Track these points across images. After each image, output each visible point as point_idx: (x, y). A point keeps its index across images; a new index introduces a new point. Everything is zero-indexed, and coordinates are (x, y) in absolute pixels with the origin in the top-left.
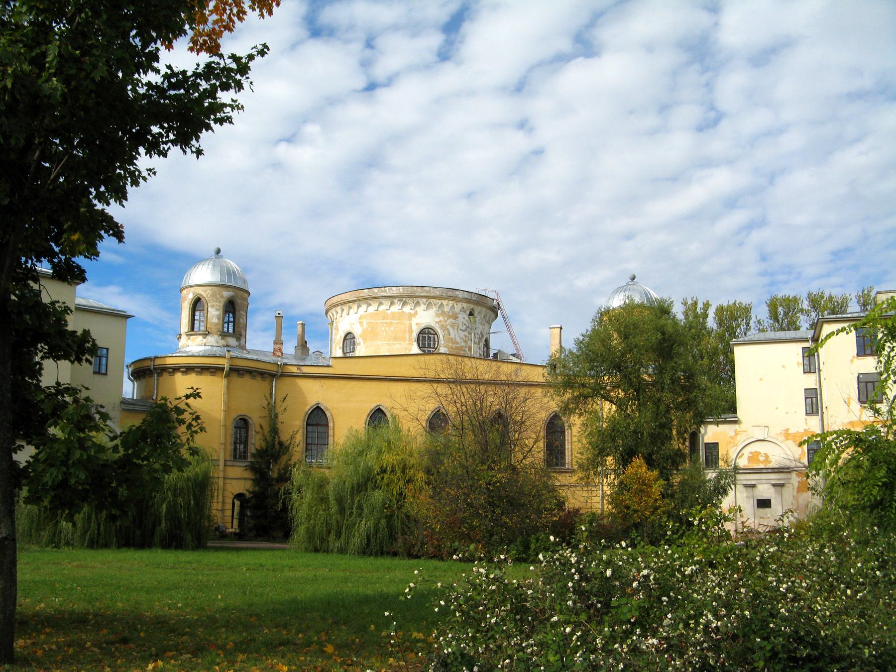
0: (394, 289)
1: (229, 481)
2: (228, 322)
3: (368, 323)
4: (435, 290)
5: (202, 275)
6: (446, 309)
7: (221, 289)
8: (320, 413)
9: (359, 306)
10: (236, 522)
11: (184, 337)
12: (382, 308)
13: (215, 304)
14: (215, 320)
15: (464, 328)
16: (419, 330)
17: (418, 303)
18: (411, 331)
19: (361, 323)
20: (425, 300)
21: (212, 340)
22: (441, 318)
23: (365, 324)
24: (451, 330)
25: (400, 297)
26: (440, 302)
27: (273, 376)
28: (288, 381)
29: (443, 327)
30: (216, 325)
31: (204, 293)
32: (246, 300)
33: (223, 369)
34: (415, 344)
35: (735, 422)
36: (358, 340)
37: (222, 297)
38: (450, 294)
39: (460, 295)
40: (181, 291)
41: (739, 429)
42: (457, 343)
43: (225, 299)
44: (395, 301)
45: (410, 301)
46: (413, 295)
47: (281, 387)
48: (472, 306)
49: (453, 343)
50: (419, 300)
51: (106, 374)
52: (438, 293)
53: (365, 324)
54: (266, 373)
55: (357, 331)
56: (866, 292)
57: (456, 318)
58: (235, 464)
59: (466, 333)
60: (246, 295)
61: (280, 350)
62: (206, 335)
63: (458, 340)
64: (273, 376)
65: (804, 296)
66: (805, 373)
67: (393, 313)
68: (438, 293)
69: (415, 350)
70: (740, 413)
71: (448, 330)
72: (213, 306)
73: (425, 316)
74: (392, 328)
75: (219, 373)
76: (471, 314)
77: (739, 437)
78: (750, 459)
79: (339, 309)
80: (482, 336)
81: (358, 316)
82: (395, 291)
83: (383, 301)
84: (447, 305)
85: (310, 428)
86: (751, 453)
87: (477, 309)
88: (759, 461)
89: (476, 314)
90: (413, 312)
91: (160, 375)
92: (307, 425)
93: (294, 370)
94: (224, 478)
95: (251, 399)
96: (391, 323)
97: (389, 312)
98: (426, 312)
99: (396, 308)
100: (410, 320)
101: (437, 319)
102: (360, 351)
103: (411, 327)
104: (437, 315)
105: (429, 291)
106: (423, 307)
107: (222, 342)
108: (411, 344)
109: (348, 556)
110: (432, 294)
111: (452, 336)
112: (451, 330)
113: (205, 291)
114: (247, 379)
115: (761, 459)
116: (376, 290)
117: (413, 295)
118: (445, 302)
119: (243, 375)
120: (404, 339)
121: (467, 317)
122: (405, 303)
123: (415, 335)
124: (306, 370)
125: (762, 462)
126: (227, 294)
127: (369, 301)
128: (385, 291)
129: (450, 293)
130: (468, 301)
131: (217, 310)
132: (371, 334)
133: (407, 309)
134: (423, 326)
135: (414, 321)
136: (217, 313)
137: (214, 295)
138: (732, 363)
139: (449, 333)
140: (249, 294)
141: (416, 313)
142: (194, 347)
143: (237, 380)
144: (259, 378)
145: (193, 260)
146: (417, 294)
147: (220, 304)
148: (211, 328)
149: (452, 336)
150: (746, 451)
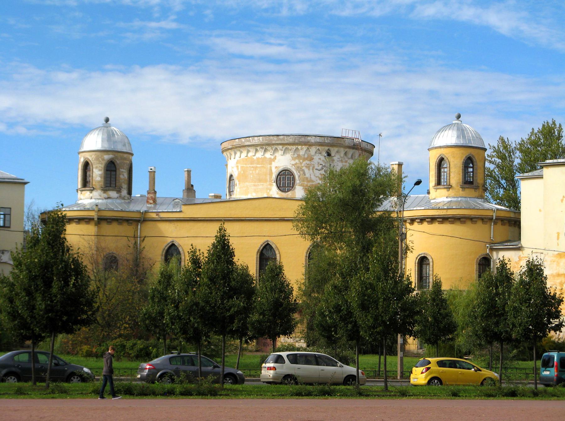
0: (256, 138)
3: (242, 167)
4: (289, 138)
5: (94, 142)
6: (302, 153)
7: (102, 153)
9: (235, 153)
12: (250, 154)
13: (98, 165)
14: (98, 179)
16: (278, 173)
17: (276, 150)
18: (271, 173)
19: (237, 167)
20: (281, 147)
21: (96, 194)
22: (297, 161)
23: (239, 167)
24: (306, 171)
25: (261, 145)
26: (294, 147)
27: (138, 221)
28: (150, 224)
29: (299, 169)
30: (99, 182)
31: (91, 157)
34: (275, 184)
35: (519, 249)
37: (103, 160)
38: (301, 141)
39: (313, 140)
40: (79, 153)
41: (522, 256)
42: (313, 181)
44: (258, 148)
45: (269, 148)
46: (271, 143)
47: (147, 229)
48: (327, 148)
49: (308, 182)
50: (276, 146)
51: (9, 227)
52: (291, 140)
53: (239, 167)
54: (475, 218)
57: (311, 159)
62: (449, 188)
63: (313, 178)
64: (138, 221)
66: (268, 244)
67: (258, 159)
68: (291, 140)
69: (275, 192)
70: (524, 242)
71: (303, 170)
72: (96, 168)
73: (283, 160)
74: (257, 172)
76: (329, 155)
81: (236, 160)
82: (256, 141)
83: (250, 149)
84: (303, 150)
90: (272, 157)
93: (154, 216)
95: (117, 241)
96: (256, 167)
97: (255, 158)
98: (283, 157)
99: (260, 154)
100: (271, 164)
101: (293, 162)
104: (294, 159)
105: (283, 139)
106: (280, 152)
107: (105, 195)
108: (271, 185)
110: (286, 142)
111: (307, 175)
112: (306, 171)
113: (91, 156)
116: (243, 140)
117: (271, 143)
118: (299, 147)
120: (266, 181)
122: (266, 151)
123: (274, 176)
124: (163, 215)
126: (107, 157)
128: (249, 141)
129: (303, 139)
130: (321, 144)
131: (100, 170)
132: (244, 176)
133: (268, 155)
134: (281, 169)
135: (274, 165)
136: (100, 173)
137: (97, 159)
139: (304, 174)
140: (132, 154)
141: (275, 158)
142: (88, 199)
143: (105, 226)
144: (125, 224)
145: (84, 130)
146: (274, 142)
147: (102, 166)
149: (307, 175)
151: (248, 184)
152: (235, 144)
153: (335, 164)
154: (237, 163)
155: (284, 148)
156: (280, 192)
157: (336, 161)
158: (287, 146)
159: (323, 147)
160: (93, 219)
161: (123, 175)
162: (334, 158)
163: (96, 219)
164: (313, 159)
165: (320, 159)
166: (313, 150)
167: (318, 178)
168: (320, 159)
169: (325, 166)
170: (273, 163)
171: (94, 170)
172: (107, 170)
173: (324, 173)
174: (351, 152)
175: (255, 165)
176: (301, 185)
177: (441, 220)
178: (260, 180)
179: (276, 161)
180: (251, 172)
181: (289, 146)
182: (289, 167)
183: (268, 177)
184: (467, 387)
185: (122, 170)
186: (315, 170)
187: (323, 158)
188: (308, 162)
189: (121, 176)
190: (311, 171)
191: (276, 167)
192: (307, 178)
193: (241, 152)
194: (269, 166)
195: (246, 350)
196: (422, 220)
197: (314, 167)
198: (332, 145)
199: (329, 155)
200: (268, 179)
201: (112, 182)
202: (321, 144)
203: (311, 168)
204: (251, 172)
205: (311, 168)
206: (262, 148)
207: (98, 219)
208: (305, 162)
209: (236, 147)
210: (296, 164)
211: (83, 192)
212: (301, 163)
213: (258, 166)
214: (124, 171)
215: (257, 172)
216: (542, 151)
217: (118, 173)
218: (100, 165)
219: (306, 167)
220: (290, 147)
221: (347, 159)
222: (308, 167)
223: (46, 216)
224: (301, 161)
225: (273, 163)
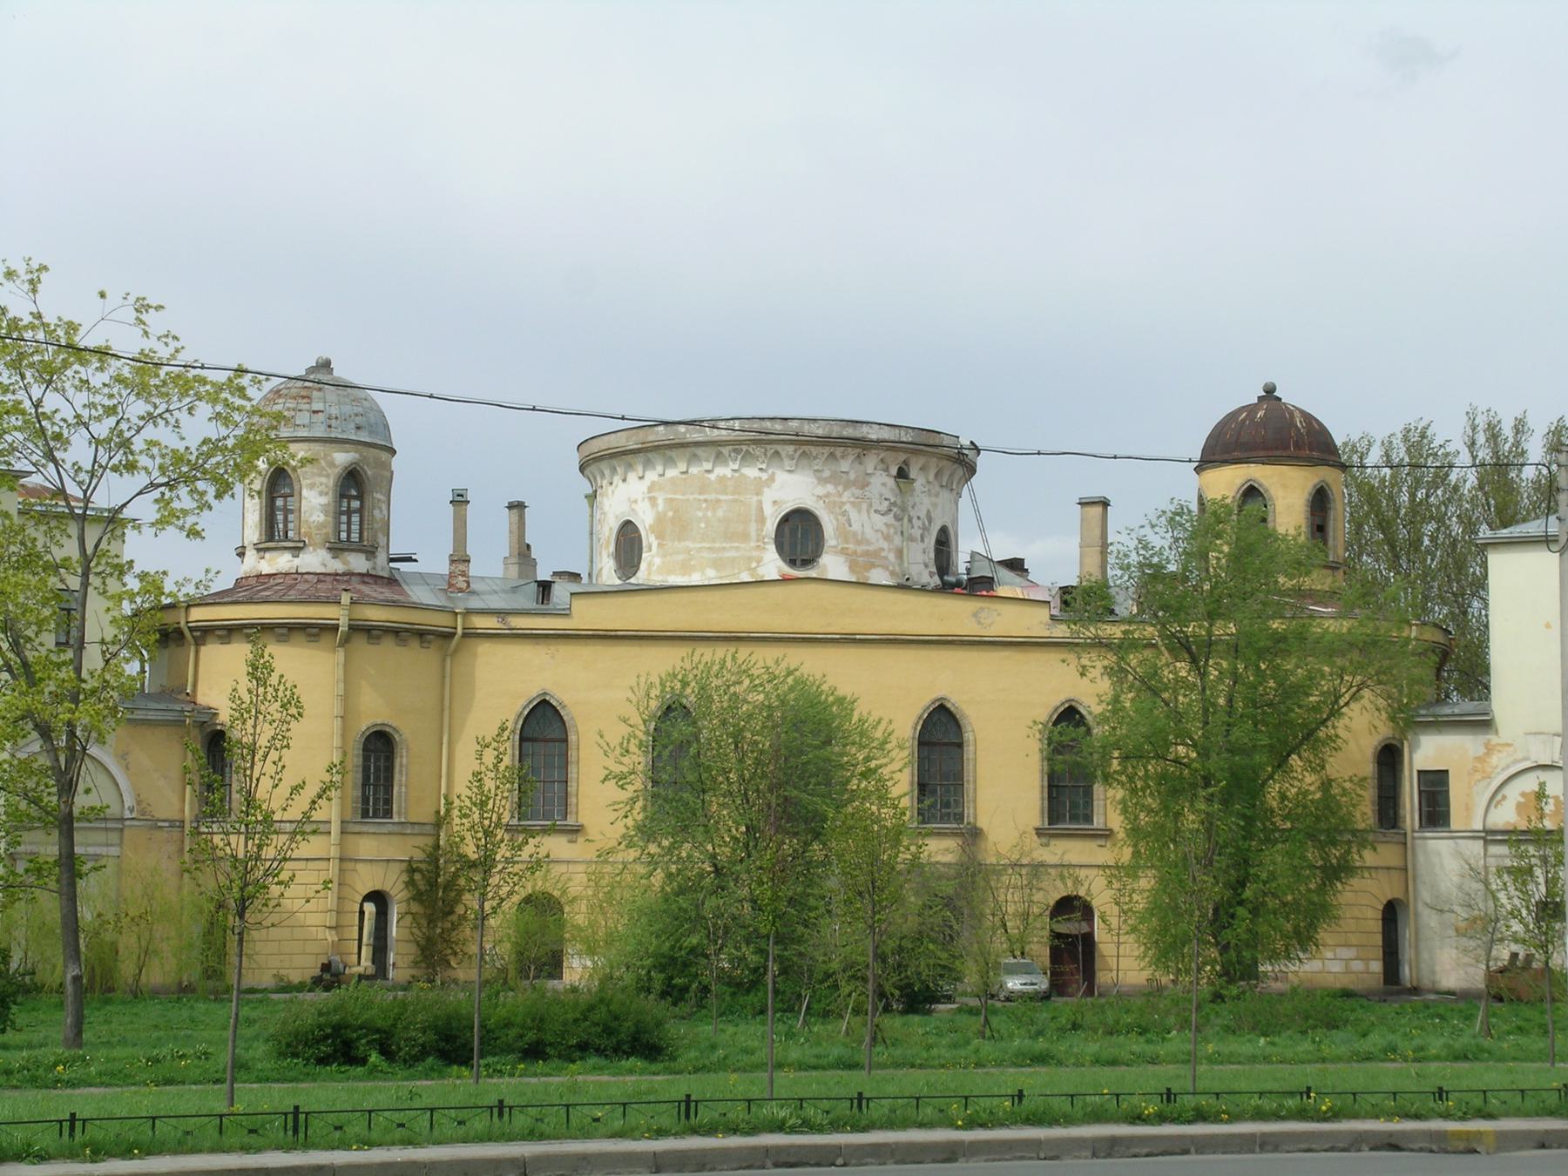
1: (350, 865)
2: (349, 513)
8: (549, 713)
10: (366, 952)
18: (761, 519)
19: (653, 500)
20: (791, 448)
22: (830, 488)
24: (853, 515)
30: (321, 526)
32: (387, 466)
33: (335, 628)
34: (772, 547)
36: (649, 539)
42: (868, 542)
43: (338, 470)
48: (903, 457)
50: (779, 448)
53: (660, 501)
55: (645, 519)
56: (325, 1049)
58: (364, 828)
60: (384, 456)
61: (464, 574)
63: (869, 534)
67: (721, 479)
69: (772, 565)
71: (844, 513)
72: (312, 486)
73: (792, 487)
74: (720, 513)
75: (326, 639)
76: (902, 474)
77: (1494, 760)
79: (604, 466)
80: (930, 519)
83: (700, 451)
85: (528, 746)
86: (1523, 794)
90: (764, 476)
91: (199, 642)
92: (522, 739)
94: (341, 860)
97: (712, 476)
101: (820, 491)
102: (646, 574)
103: (761, 509)
114: (388, 644)
119: (378, 638)
120: (745, 537)
121: (891, 482)
123: (771, 526)
127: (668, 453)
129: (849, 432)
131: (321, 494)
132: (675, 525)
133: (751, 472)
135: (768, 496)
136: (324, 500)
138: (1481, 584)
144: (415, 643)
147: (329, 481)
148: (308, 535)
149: (856, 527)
150: (1514, 792)
151: (690, 544)
152: (651, 438)
153: (917, 500)
154: (650, 489)
157: (918, 491)
163: (343, 628)
164: (868, 484)
165: (884, 484)
166: (871, 461)
169: (894, 504)
170: (766, 490)
171: (305, 492)
175: (713, 496)
176: (844, 552)
177: (284, 631)
178: (729, 537)
179: (776, 485)
180: (700, 514)
181: (812, 448)
183: (753, 528)
185: (378, 496)
186: (873, 514)
188: (858, 492)
191: (775, 502)
192: (855, 534)
194: (755, 498)
195: (27, 991)
196: (397, 633)
199: (902, 474)
200: (753, 534)
204: (700, 514)
206: (737, 451)
207: (351, 627)
210: (828, 495)
211: (267, 555)
213: (723, 497)
215: (720, 513)
218: (323, 480)
219: (852, 503)
225: (766, 490)
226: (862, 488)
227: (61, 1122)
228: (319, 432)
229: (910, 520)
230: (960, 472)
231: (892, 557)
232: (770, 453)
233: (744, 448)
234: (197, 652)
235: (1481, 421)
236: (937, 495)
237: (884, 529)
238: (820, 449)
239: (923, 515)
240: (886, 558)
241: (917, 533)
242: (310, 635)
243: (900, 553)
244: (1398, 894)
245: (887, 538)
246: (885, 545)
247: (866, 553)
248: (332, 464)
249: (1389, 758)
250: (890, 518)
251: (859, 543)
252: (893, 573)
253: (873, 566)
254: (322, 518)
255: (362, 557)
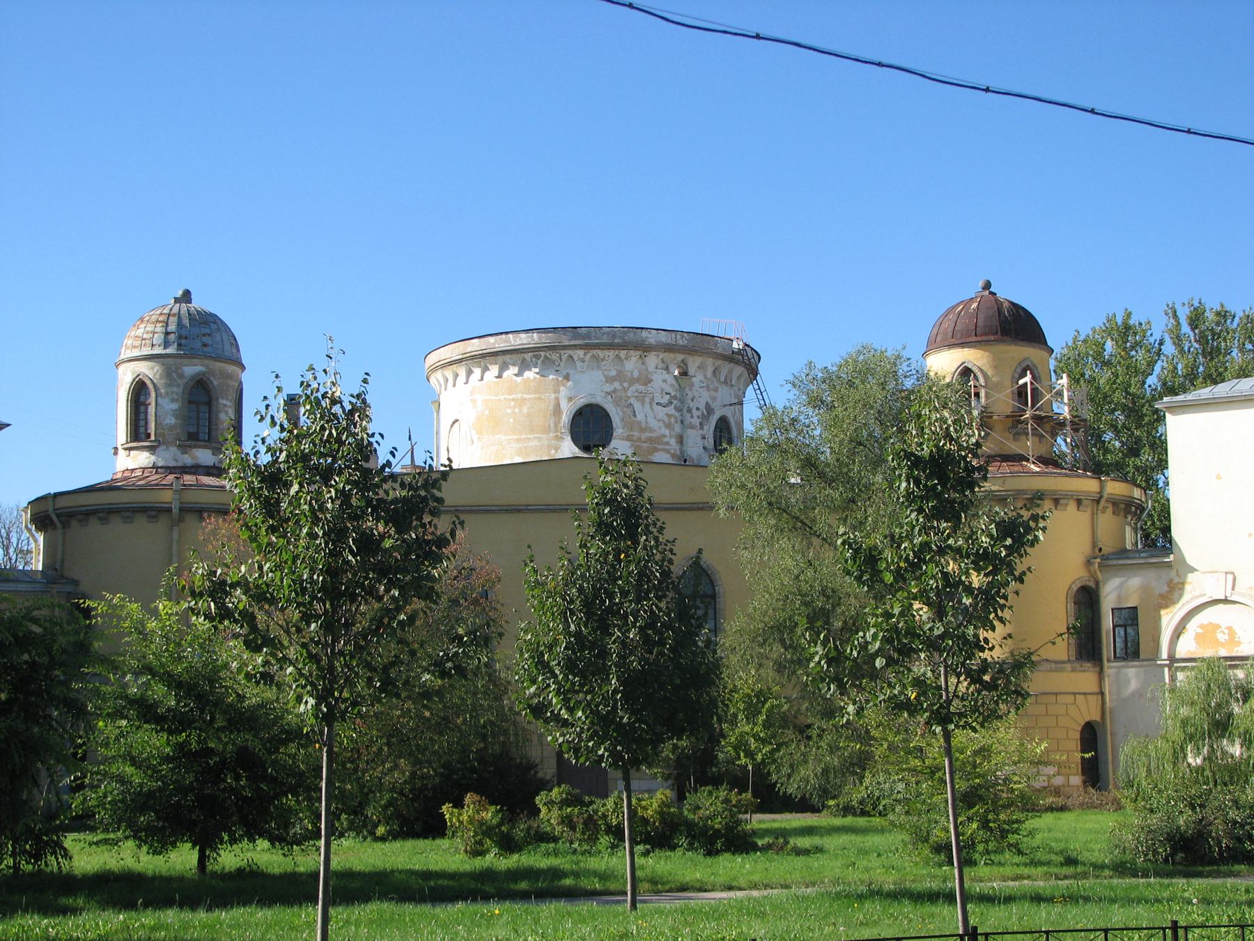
0: (523, 335)
11: (121, 452)
15: (666, 399)
19: (474, 401)
20: (581, 353)
24: (637, 406)
30: (172, 428)
33: (169, 510)
39: (652, 339)
40: (117, 366)
42: (651, 430)
48: (680, 357)
50: (570, 352)
59: (671, 410)
60: (231, 368)
63: (653, 423)
65: (1240, 314)
69: (568, 449)
78: (1199, 638)
86: (1201, 626)
87: (694, 363)
88: (1216, 642)
89: (691, 371)
101: (608, 388)
103: (558, 406)
109: (679, 852)
115: (1222, 637)
118: (623, 354)
123: (566, 418)
125: (1222, 645)
131: (173, 400)
136: (175, 406)
138: (1160, 447)
149: (640, 417)
150: (1193, 626)
152: (469, 349)
153: (696, 394)
154: (472, 393)
155: (588, 356)
156: (577, 450)
157: (697, 387)
158: (594, 352)
159: (672, 355)
160: (169, 510)
161: (227, 413)
162: (693, 380)
163: (175, 511)
164: (650, 381)
165: (665, 381)
166: (652, 360)
167: (661, 424)
168: (665, 381)
169: (675, 397)
172: (190, 402)
173: (673, 412)
174: (726, 367)
181: (599, 352)
182: (599, 400)
184: (189, 479)
185: (224, 402)
186: (655, 406)
187: (671, 380)
188: (641, 388)
189: (222, 416)
190: (647, 406)
192: (639, 423)
193: (485, 369)
197: (653, 399)
198: (690, 350)
201: (201, 422)
202: (669, 348)
203: (647, 400)
205: (647, 400)
206: (538, 357)
207: (181, 510)
208: (633, 388)
209: (473, 358)
210: (615, 391)
212: (625, 390)
214: (228, 403)
216: (1220, 353)
217: (214, 409)
218: (175, 389)
220: (601, 353)
221: (716, 384)
222: (641, 398)
223: (42, 507)
224: (626, 385)
226: (645, 384)
227: (1164, 929)
228: (158, 350)
229: (689, 411)
230: (739, 370)
231: (673, 441)
232: (565, 357)
233: (543, 354)
234: (64, 534)
235: (1183, 313)
236: (716, 390)
237: (666, 419)
238: (607, 353)
239: (702, 406)
240: (667, 443)
241: (696, 421)
242: (151, 517)
243: (681, 440)
244: (1096, 717)
245: (668, 426)
246: (667, 432)
247: (650, 440)
248: (181, 376)
249: (1087, 598)
250: (671, 410)
251: (643, 430)
252: (673, 456)
253: (656, 450)
254: (173, 421)
255: (209, 452)
